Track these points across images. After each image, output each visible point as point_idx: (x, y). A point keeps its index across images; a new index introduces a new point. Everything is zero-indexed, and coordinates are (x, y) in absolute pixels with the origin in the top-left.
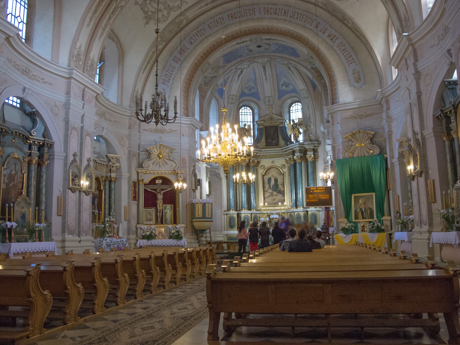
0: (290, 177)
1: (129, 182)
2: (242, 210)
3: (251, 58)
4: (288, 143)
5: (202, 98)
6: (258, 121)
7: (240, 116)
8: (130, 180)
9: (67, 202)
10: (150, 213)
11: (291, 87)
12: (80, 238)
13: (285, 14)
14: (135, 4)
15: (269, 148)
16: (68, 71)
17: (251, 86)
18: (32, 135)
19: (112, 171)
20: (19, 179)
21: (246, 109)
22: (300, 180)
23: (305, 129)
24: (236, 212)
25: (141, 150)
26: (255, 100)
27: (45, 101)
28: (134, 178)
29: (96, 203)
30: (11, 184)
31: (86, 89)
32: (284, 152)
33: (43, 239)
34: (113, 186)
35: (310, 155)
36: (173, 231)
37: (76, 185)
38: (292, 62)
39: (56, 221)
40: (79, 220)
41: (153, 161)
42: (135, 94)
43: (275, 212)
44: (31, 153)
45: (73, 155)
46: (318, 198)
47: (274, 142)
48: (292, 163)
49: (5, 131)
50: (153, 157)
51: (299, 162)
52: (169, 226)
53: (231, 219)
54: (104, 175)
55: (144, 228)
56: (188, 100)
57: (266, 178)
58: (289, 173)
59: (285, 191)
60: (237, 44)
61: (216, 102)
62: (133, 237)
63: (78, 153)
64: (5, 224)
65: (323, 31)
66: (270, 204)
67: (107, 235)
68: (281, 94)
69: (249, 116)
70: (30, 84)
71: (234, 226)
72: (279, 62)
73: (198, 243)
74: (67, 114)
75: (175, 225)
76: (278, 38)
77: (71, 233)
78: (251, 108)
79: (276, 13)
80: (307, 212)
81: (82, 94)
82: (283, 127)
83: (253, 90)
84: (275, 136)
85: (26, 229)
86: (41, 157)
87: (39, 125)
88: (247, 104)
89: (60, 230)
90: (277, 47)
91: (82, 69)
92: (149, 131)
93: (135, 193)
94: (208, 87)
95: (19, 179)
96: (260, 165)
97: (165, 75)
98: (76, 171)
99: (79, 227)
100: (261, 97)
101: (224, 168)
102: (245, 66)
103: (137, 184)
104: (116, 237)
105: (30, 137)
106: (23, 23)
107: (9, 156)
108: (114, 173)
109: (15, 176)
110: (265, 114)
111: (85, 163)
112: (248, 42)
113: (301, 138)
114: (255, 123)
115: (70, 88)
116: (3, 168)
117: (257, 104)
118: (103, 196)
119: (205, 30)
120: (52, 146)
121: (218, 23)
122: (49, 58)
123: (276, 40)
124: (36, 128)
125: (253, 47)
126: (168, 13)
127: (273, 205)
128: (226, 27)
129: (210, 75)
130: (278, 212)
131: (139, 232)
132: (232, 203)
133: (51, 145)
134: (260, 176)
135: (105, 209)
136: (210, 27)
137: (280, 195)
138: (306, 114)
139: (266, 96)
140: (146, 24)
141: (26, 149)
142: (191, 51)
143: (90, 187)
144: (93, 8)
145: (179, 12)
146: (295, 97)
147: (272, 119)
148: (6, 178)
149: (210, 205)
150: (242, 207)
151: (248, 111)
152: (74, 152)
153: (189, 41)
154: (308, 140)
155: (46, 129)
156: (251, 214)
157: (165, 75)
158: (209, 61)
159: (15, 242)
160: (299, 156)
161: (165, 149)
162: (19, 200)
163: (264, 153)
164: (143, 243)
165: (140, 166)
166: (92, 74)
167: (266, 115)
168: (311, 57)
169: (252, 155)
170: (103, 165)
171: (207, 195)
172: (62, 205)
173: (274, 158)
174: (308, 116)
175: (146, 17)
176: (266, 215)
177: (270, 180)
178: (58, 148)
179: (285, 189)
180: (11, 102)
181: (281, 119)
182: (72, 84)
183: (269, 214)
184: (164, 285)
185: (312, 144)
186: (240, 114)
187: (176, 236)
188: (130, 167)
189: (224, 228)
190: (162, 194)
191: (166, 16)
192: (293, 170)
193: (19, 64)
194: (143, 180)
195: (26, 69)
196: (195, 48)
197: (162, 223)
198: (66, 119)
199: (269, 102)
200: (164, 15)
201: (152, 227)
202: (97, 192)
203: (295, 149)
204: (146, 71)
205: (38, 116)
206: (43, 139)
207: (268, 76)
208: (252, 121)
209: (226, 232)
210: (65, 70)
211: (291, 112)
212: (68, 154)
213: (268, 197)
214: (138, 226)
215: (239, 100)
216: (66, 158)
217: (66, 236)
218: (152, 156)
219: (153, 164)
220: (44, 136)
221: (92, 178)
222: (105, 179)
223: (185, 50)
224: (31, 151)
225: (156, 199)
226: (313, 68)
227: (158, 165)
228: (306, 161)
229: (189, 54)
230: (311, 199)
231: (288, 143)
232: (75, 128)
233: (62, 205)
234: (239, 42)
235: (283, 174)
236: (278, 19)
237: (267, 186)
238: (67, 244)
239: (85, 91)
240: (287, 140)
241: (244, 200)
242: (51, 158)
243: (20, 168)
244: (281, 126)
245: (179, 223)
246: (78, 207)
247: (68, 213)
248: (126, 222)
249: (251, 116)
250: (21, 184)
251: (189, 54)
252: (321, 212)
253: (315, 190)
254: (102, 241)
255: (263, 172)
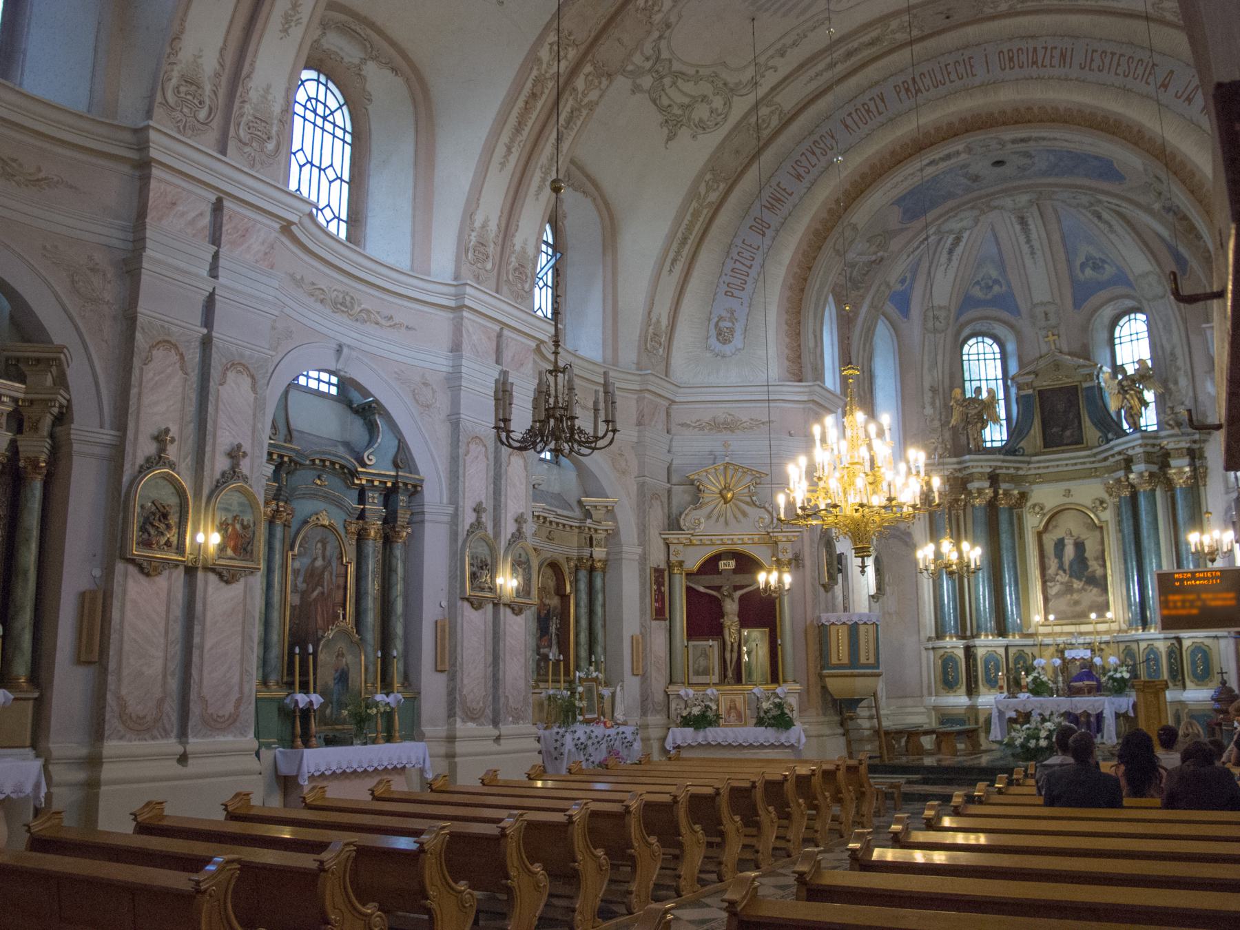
0: (1120, 535)
1: (642, 570)
2: (978, 636)
3: (980, 198)
4: (1110, 436)
5: (845, 323)
6: (1019, 375)
7: (966, 364)
8: (645, 565)
9: (459, 636)
10: (706, 654)
11: (1109, 271)
12: (499, 729)
13: (1064, 60)
14: (633, 92)
15: (1054, 453)
16: (452, 290)
17: (991, 278)
18: (364, 465)
19: (594, 543)
20: (334, 578)
21: (981, 345)
22: (1153, 545)
23: (1161, 390)
24: (961, 644)
25: (674, 479)
26: (1005, 315)
27: (396, 373)
28: (657, 558)
29: (553, 629)
30: (315, 593)
31: (506, 332)
32: (1099, 461)
33: (397, 734)
34: (598, 583)
35: (1180, 469)
36: (765, 705)
37: (482, 589)
38: (1104, 198)
39: (432, 685)
40: (496, 680)
41: (706, 510)
42: (651, 330)
43: (1081, 640)
44: (363, 510)
45: (475, 510)
46: (1199, 603)
47: (1068, 433)
48: (1126, 493)
49: (291, 460)
50: (706, 500)
51: (1145, 491)
52: (756, 690)
53: (947, 662)
54: (574, 553)
55: (687, 695)
56: (799, 334)
57: (1049, 540)
58: (1120, 523)
59: (1109, 579)
60: (931, 163)
61: (892, 330)
62: (656, 719)
63: (488, 505)
64: (292, 699)
65: (1185, 96)
66: (1063, 618)
67: (580, 718)
68: (1082, 293)
69: (990, 364)
70: (355, 335)
71: (957, 683)
72: (1063, 202)
73: (844, 735)
74: (455, 403)
75: (773, 686)
76: (1058, 135)
77: (472, 716)
78: (996, 339)
79: (1035, 63)
80: (1179, 640)
81: (494, 347)
82: (1092, 388)
83: (996, 288)
84: (1071, 415)
85: (345, 713)
86: (389, 520)
87: (385, 439)
88: (984, 329)
89: (442, 711)
90: (1052, 158)
91: (494, 280)
92: (695, 427)
93: (660, 596)
94: (862, 291)
95: (334, 578)
96: (1029, 504)
97: (732, 271)
98: (483, 551)
99: (496, 699)
100: (1024, 306)
101: (855, 543)
102: (965, 223)
103: (666, 573)
104: (605, 723)
105: (360, 469)
106: (342, 180)
107: (306, 522)
108: (601, 547)
109: (323, 573)
110: (1038, 355)
111: (509, 528)
112: (963, 156)
113: (1149, 419)
114: (1009, 382)
115: (461, 336)
116: (290, 554)
117: (1012, 327)
118: (572, 611)
119: (833, 137)
120: (419, 489)
121: (868, 111)
122: (404, 263)
123: (1044, 139)
124: (376, 446)
125: (981, 166)
126: (725, 104)
127: (1073, 621)
128: (891, 120)
129: (865, 258)
130: (1088, 640)
131: (673, 705)
132: (950, 619)
133: (415, 486)
134: (1030, 533)
135: (577, 644)
136: (847, 127)
137: (1095, 591)
138: (1162, 347)
139: (1035, 301)
140: (669, 139)
141: (351, 502)
142: (801, 198)
143: (524, 591)
144: (513, 120)
145: (751, 99)
146: (1127, 296)
147: (1057, 366)
148: (300, 579)
149: (871, 629)
150: (978, 627)
151: (988, 349)
152: (478, 500)
153: (792, 171)
154: (1171, 422)
155: (402, 446)
156: (1007, 648)
157: (732, 271)
158: (854, 220)
159: (321, 746)
160: (1146, 474)
161: (740, 474)
162: (330, 634)
163: (1039, 468)
164: (684, 738)
165: (673, 524)
166: (523, 289)
167: (1041, 357)
168: (1157, 178)
169: (937, 501)
170: (568, 529)
171: (873, 596)
172: (447, 641)
173: (1069, 480)
174: (1168, 350)
175: (666, 121)
176: (1052, 649)
177: (1060, 545)
178: (434, 495)
179: (1109, 572)
180: (313, 384)
181: (1084, 366)
182: (466, 321)
183: (1062, 646)
184: (678, 886)
185: (1183, 434)
186: (965, 357)
187: (774, 717)
188: (643, 530)
189: (929, 687)
190: (737, 601)
191: (720, 111)
192: (1130, 513)
193: (323, 287)
194: (681, 563)
195: (344, 298)
196: (809, 188)
197: (739, 680)
198: (453, 417)
199: (1047, 319)
200: (717, 109)
201: (709, 692)
202: (554, 602)
203: (1130, 452)
204: (679, 267)
205: (380, 414)
206: (393, 473)
207: (1036, 244)
208: (1000, 376)
209: (933, 700)
210: (445, 289)
211: (1117, 341)
212: (461, 509)
213: (1058, 595)
214: (672, 689)
215: (957, 319)
216: (455, 518)
217: (459, 724)
218: (706, 495)
219: (709, 517)
220: (396, 466)
221: (530, 567)
222: (576, 566)
223: (782, 198)
224: (364, 504)
225: (721, 614)
226: (1169, 210)
227: (722, 519)
228: (1169, 485)
229: (795, 206)
230: (1175, 608)
231: (1110, 436)
232: (476, 437)
233: (447, 645)
234: (937, 157)
235: (1101, 528)
236: (1043, 78)
237: (1053, 564)
238: (460, 747)
239: (504, 338)
240: (1109, 427)
241: (984, 606)
242: (417, 520)
243: (336, 554)
244: (1085, 385)
245: (785, 681)
246: (490, 648)
247: (462, 664)
248: (637, 680)
249: (999, 363)
250: (341, 592)
251: (795, 206)
252: (1223, 642)
253: (1188, 579)
254: (563, 736)
255: (1040, 522)
